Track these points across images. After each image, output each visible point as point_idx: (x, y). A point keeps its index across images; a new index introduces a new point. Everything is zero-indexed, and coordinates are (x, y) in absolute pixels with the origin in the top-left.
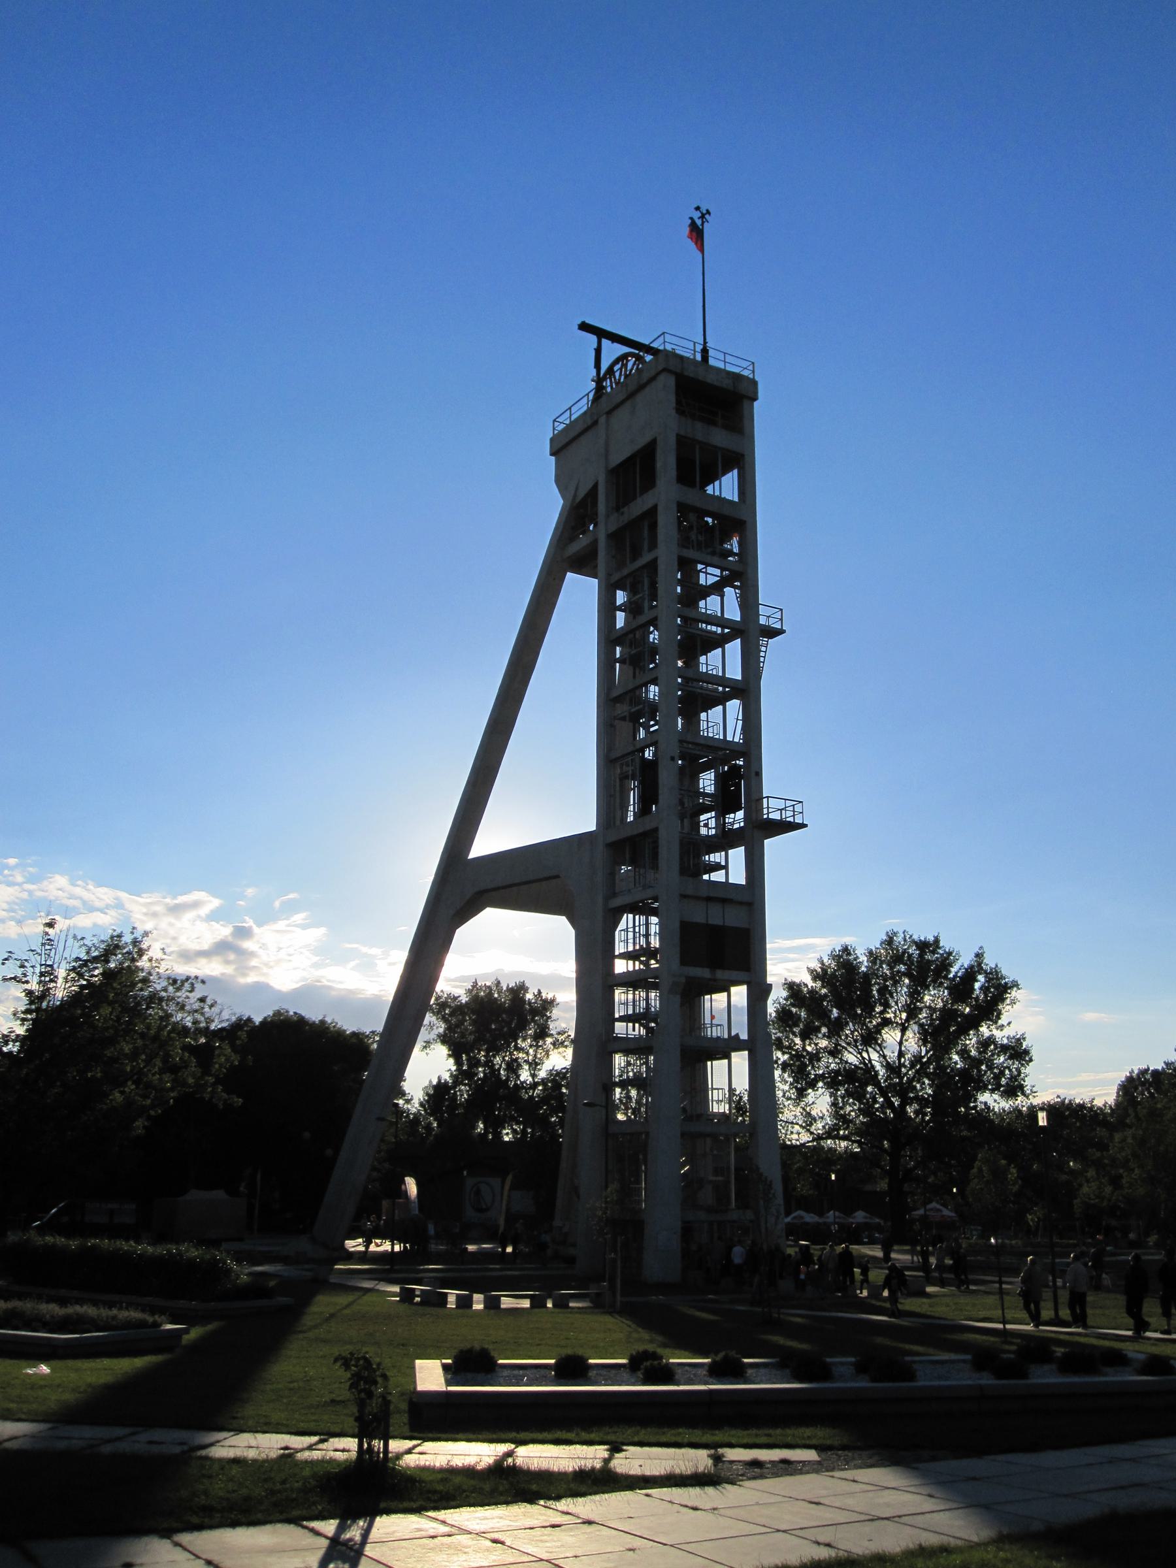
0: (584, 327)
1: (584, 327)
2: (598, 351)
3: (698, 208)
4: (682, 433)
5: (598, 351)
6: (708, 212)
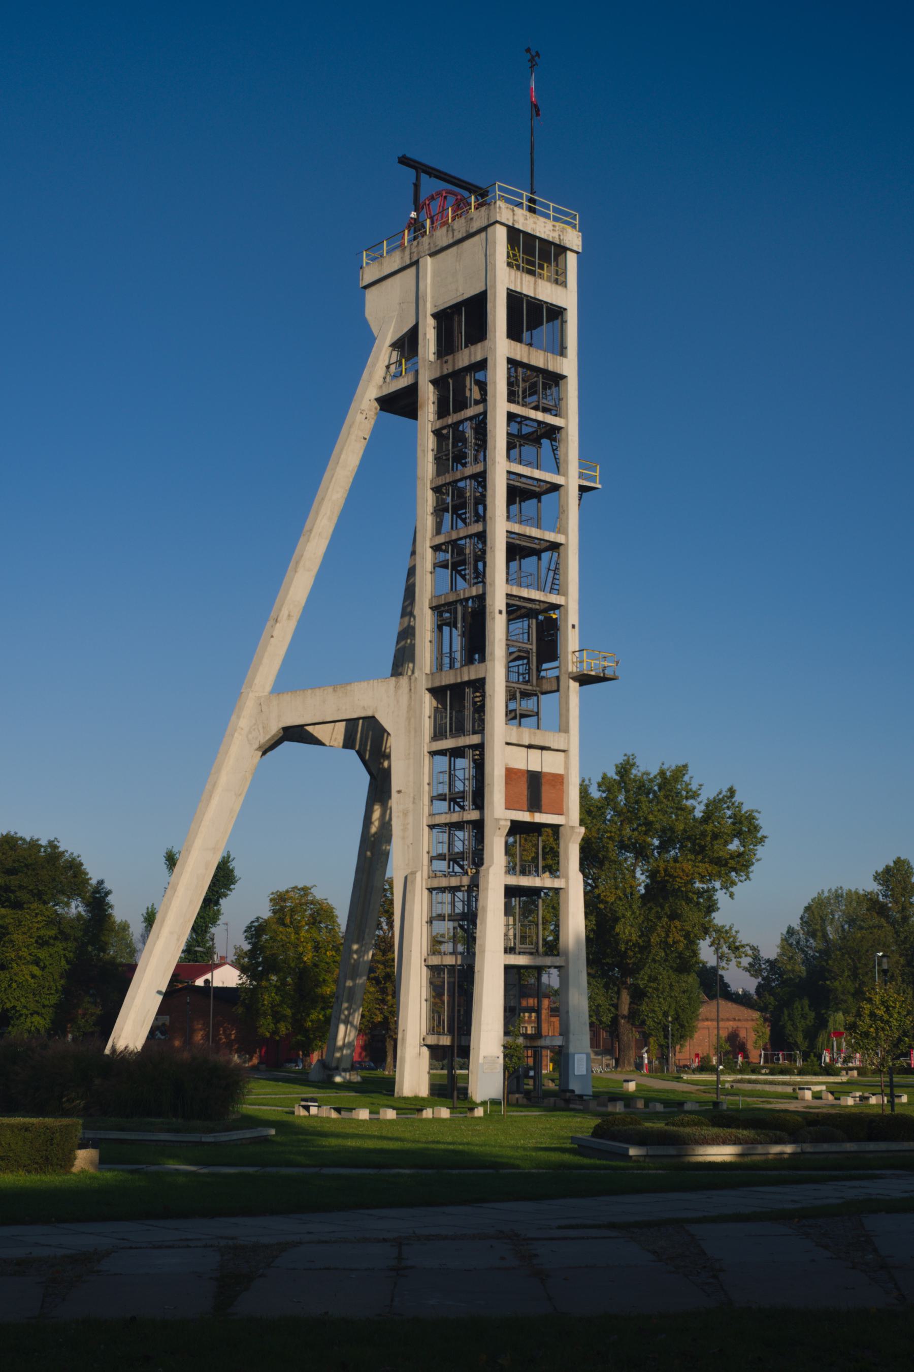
0: (405, 161)
1: (405, 161)
2: (417, 186)
3: (528, 50)
4: (512, 356)
5: (417, 186)
6: (538, 54)
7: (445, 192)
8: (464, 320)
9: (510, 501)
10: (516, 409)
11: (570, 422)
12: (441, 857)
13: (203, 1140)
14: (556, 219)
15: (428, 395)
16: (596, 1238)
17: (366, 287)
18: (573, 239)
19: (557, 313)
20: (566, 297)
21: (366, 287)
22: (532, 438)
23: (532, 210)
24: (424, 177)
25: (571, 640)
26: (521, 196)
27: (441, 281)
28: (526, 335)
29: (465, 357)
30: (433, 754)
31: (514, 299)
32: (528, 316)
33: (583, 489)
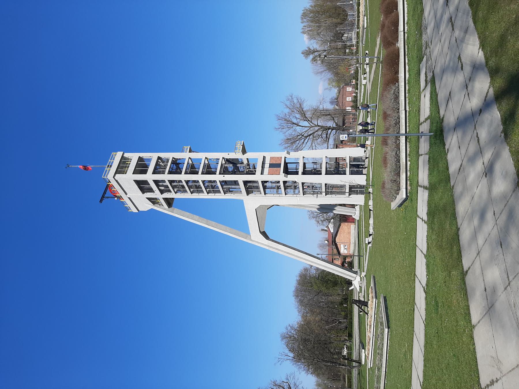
0: (101, 201)
1: (101, 201)
2: (108, 198)
7: (107, 192)
8: (143, 186)
9: (159, 173)
10: (167, 171)
11: (169, 156)
12: (294, 192)
13: (421, 159)
14: (114, 160)
15: (167, 195)
16: (376, 293)
17: (138, 210)
18: (119, 154)
19: (140, 159)
20: (134, 157)
21: (138, 210)
22: (176, 167)
23: (111, 166)
24: (106, 196)
25: (232, 156)
26: (107, 170)
27: (134, 192)
28: (197, 170)
29: (153, 186)
30: (265, 194)
31: (154, 173)
32: (142, 167)
33: (190, 151)
